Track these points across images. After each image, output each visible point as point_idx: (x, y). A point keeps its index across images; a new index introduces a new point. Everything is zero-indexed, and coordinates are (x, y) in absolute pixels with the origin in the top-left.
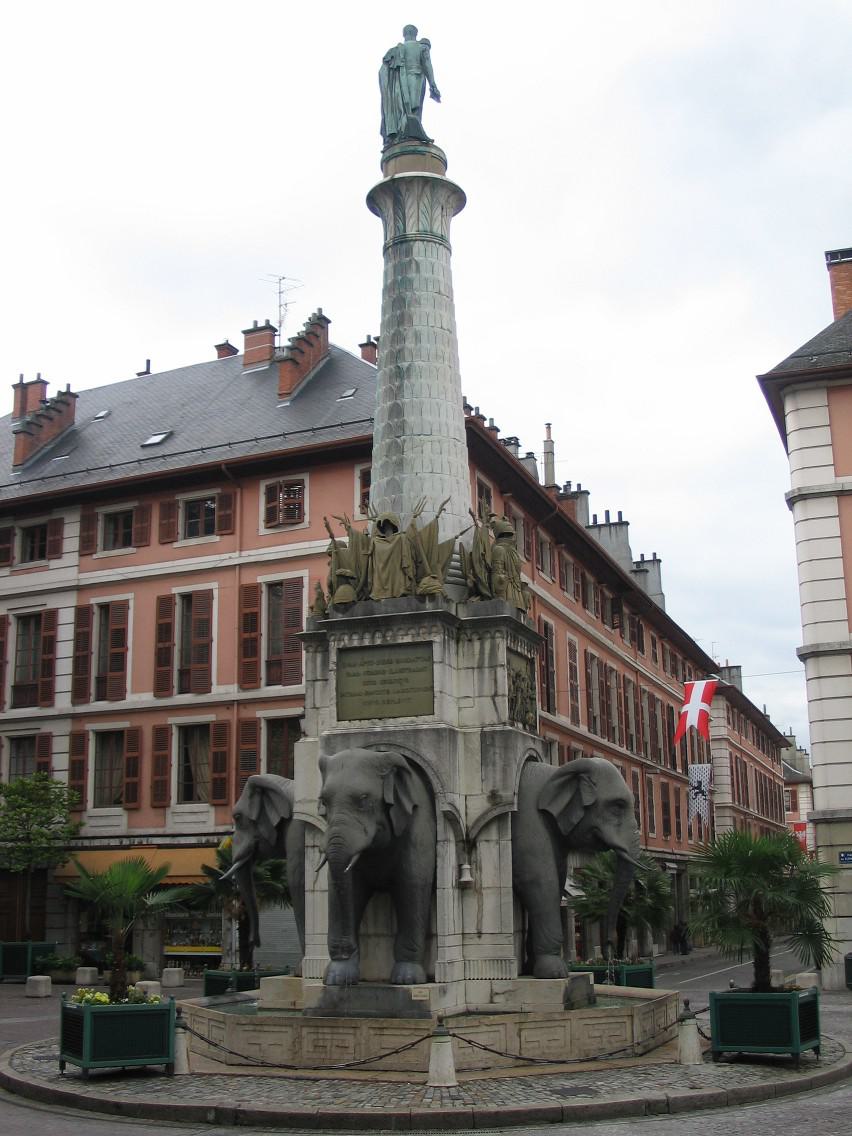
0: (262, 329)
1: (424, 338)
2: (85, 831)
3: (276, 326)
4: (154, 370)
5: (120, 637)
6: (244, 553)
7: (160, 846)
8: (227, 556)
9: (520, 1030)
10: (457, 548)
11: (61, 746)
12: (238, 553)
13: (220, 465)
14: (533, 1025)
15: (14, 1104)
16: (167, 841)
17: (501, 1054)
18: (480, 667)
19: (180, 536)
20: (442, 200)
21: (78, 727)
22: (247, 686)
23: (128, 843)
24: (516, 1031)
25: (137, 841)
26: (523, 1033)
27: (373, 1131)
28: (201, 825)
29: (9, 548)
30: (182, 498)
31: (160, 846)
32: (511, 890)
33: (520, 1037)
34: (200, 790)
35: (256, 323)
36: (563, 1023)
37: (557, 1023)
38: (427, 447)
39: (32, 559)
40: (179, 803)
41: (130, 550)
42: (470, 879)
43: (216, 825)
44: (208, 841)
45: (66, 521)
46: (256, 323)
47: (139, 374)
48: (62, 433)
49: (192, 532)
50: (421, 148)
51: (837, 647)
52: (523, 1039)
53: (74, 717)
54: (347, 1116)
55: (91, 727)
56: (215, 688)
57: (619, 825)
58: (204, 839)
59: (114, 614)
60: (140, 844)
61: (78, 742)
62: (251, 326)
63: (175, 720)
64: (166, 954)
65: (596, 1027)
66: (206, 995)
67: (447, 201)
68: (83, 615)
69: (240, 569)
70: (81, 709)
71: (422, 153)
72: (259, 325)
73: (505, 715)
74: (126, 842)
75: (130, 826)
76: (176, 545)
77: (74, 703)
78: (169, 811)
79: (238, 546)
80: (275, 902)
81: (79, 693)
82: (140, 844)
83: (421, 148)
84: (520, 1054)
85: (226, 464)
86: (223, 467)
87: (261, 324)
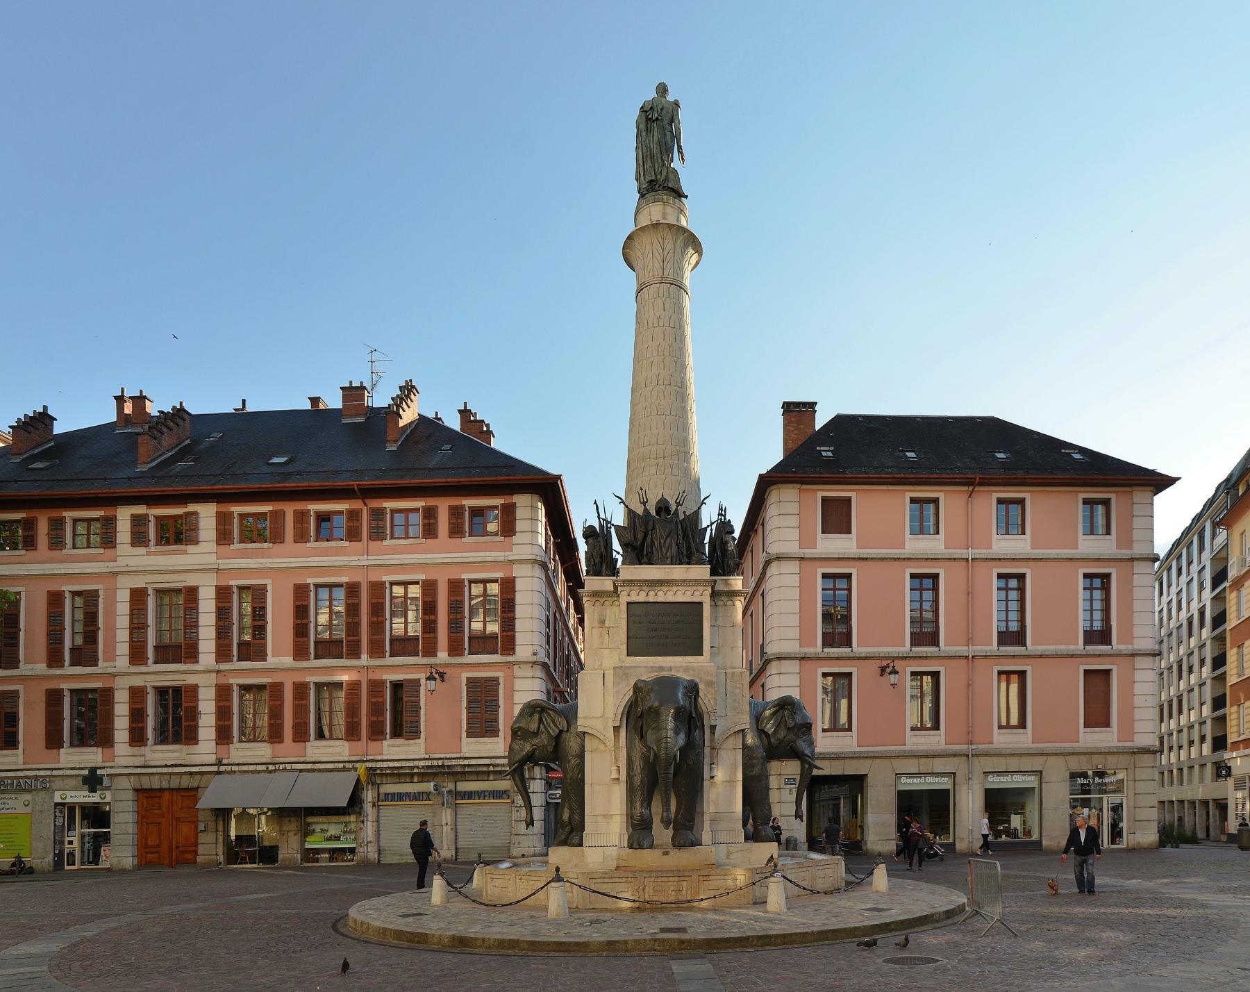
0: (356, 388)
5: (259, 613)
6: (370, 557)
8: (356, 558)
12: (366, 556)
15: (11, 882)
21: (223, 681)
23: (274, 768)
25: (282, 767)
41: (266, 545)
44: (344, 767)
48: (180, 444)
51: (793, 656)
58: (341, 766)
59: (258, 593)
60: (285, 769)
64: (306, 847)
66: (236, 836)
68: (223, 593)
74: (271, 767)
76: (309, 545)
79: (366, 551)
81: (223, 653)
82: (285, 769)
84: (139, 778)
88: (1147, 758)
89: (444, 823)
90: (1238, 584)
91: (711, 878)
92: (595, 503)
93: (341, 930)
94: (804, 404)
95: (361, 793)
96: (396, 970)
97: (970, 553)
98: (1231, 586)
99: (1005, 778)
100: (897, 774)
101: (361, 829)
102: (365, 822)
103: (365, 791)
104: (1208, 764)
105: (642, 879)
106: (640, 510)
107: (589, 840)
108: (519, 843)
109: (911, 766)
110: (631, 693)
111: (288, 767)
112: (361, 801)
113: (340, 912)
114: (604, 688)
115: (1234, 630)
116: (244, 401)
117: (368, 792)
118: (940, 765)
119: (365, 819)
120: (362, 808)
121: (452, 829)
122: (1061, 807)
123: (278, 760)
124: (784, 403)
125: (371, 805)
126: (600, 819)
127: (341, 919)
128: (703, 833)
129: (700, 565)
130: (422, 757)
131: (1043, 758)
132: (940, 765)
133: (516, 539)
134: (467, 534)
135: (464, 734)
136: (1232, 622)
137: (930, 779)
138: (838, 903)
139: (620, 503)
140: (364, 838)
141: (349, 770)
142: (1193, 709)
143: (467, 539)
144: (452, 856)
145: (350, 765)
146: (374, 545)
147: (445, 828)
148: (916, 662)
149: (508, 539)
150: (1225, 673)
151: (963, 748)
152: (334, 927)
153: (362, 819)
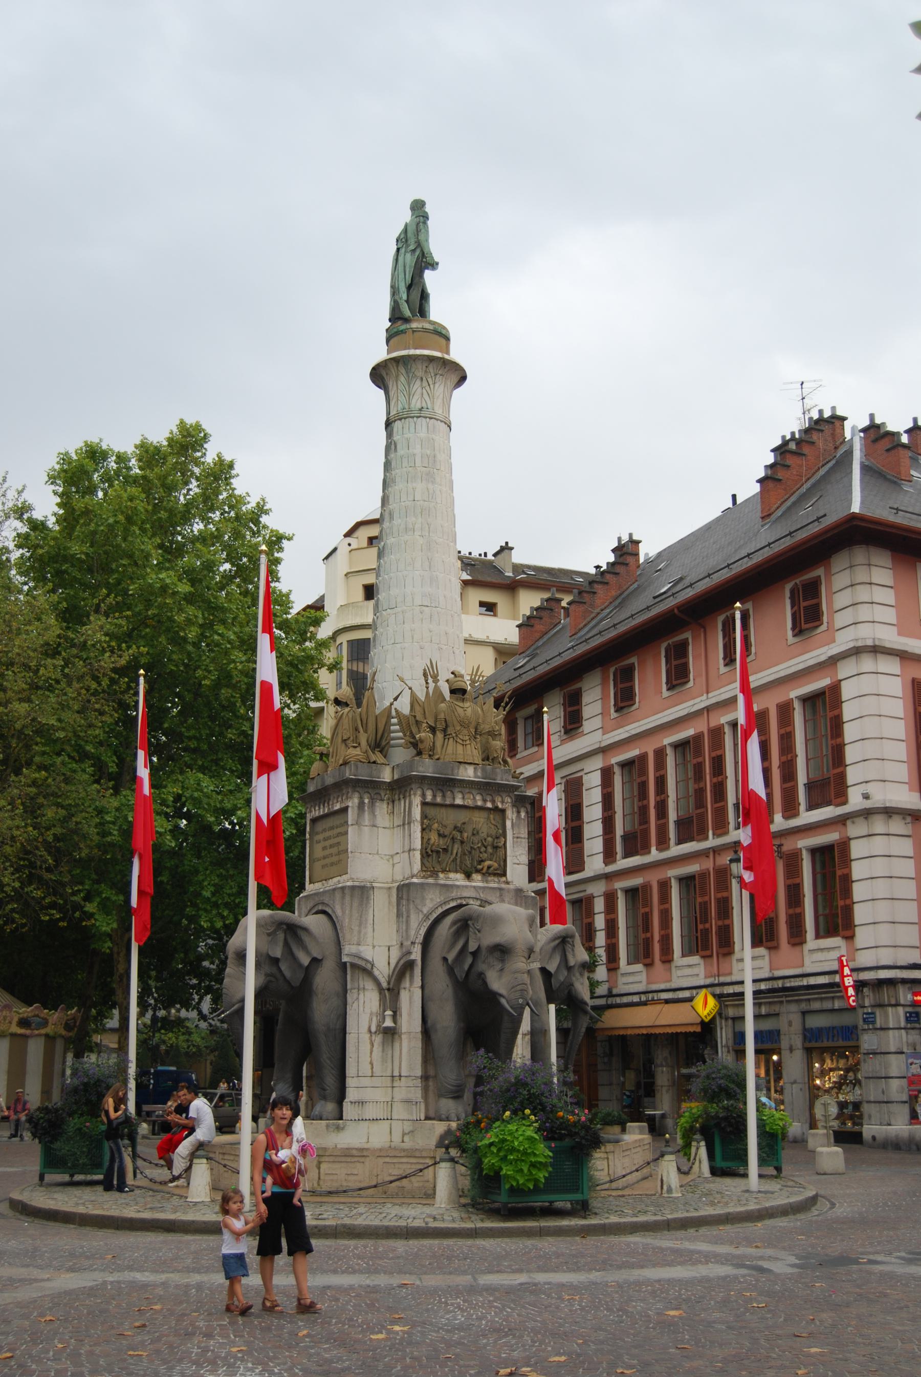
1: (396, 515)
2: (621, 988)
6: (710, 695)
7: (667, 1001)
9: (320, 1163)
10: (394, 713)
11: (599, 905)
13: (673, 610)
14: (331, 1159)
17: (375, 1186)
18: (404, 824)
20: (419, 373)
22: (719, 832)
24: (315, 1163)
26: (323, 1166)
27: (72, 1226)
28: (695, 978)
31: (667, 1001)
32: (420, 1036)
33: (319, 1168)
35: (619, 539)
36: (362, 1159)
37: (356, 1159)
38: (392, 619)
40: (683, 956)
42: (392, 1025)
43: (706, 977)
48: (621, 594)
50: (403, 327)
52: (322, 1170)
53: (608, 877)
54: (74, 1214)
55: (620, 885)
57: (502, 970)
60: (653, 1000)
61: (610, 899)
63: (673, 873)
65: (397, 1166)
67: (426, 372)
69: (708, 711)
70: (611, 868)
71: (403, 332)
73: (417, 866)
74: (643, 998)
75: (648, 983)
77: (606, 863)
78: (673, 964)
81: (609, 855)
82: (653, 1000)
83: (403, 327)
85: (678, 608)
86: (676, 611)
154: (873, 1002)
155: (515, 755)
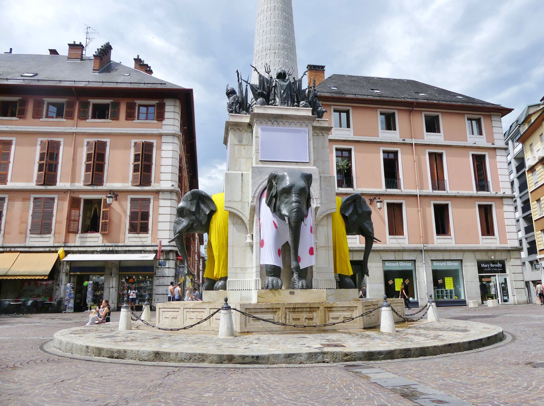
3: (84, 46)
4: (13, 52)
6: (78, 128)
12: (75, 127)
16: (27, 249)
19: (90, 117)
29: (72, 111)
30: (93, 101)
31: (21, 252)
34: (533, 234)
39: (425, 116)
41: (14, 118)
45: (166, 104)
46: (75, 42)
47: (5, 53)
49: (94, 117)
56: (58, 183)
58: (47, 249)
62: (72, 43)
72: (76, 43)
80: (486, 300)
87: (78, 43)
88: (515, 254)
89: (111, 286)
90: (532, 169)
91: (334, 309)
92: (237, 71)
93: (47, 350)
94: (319, 67)
95: (59, 267)
96: (109, 381)
97: (414, 141)
98: (528, 171)
99: (443, 263)
100: (383, 260)
101: (57, 289)
102: (60, 285)
103: (62, 265)
104: (526, 262)
105: (284, 309)
106: (266, 76)
107: (235, 286)
108: (158, 299)
109: (391, 256)
110: (266, 182)
111: (13, 250)
112: (59, 272)
113: (44, 338)
114: (242, 182)
115: (533, 193)
116: (11, 49)
117: (64, 266)
118: (406, 256)
119: (60, 283)
120: (58, 276)
121: (116, 290)
122: (474, 280)
123: (5, 245)
124: (308, 66)
125: (65, 274)
126: (238, 271)
127: (45, 342)
128: (313, 280)
129: (306, 107)
130: (100, 245)
131: (461, 254)
132: (406, 256)
133: (164, 122)
134: (136, 118)
135: (28, 232)
136: (531, 187)
137: (402, 264)
138: (406, 332)
139: (254, 70)
140: (58, 296)
141: (53, 252)
142: (520, 231)
143: (136, 121)
144: (115, 308)
145: (54, 249)
146: (81, 122)
147: (111, 289)
148: (391, 197)
149: (160, 123)
150: (531, 214)
151: (420, 246)
152: (41, 348)
153: (58, 283)
154: (165, 258)
155: (162, 121)
